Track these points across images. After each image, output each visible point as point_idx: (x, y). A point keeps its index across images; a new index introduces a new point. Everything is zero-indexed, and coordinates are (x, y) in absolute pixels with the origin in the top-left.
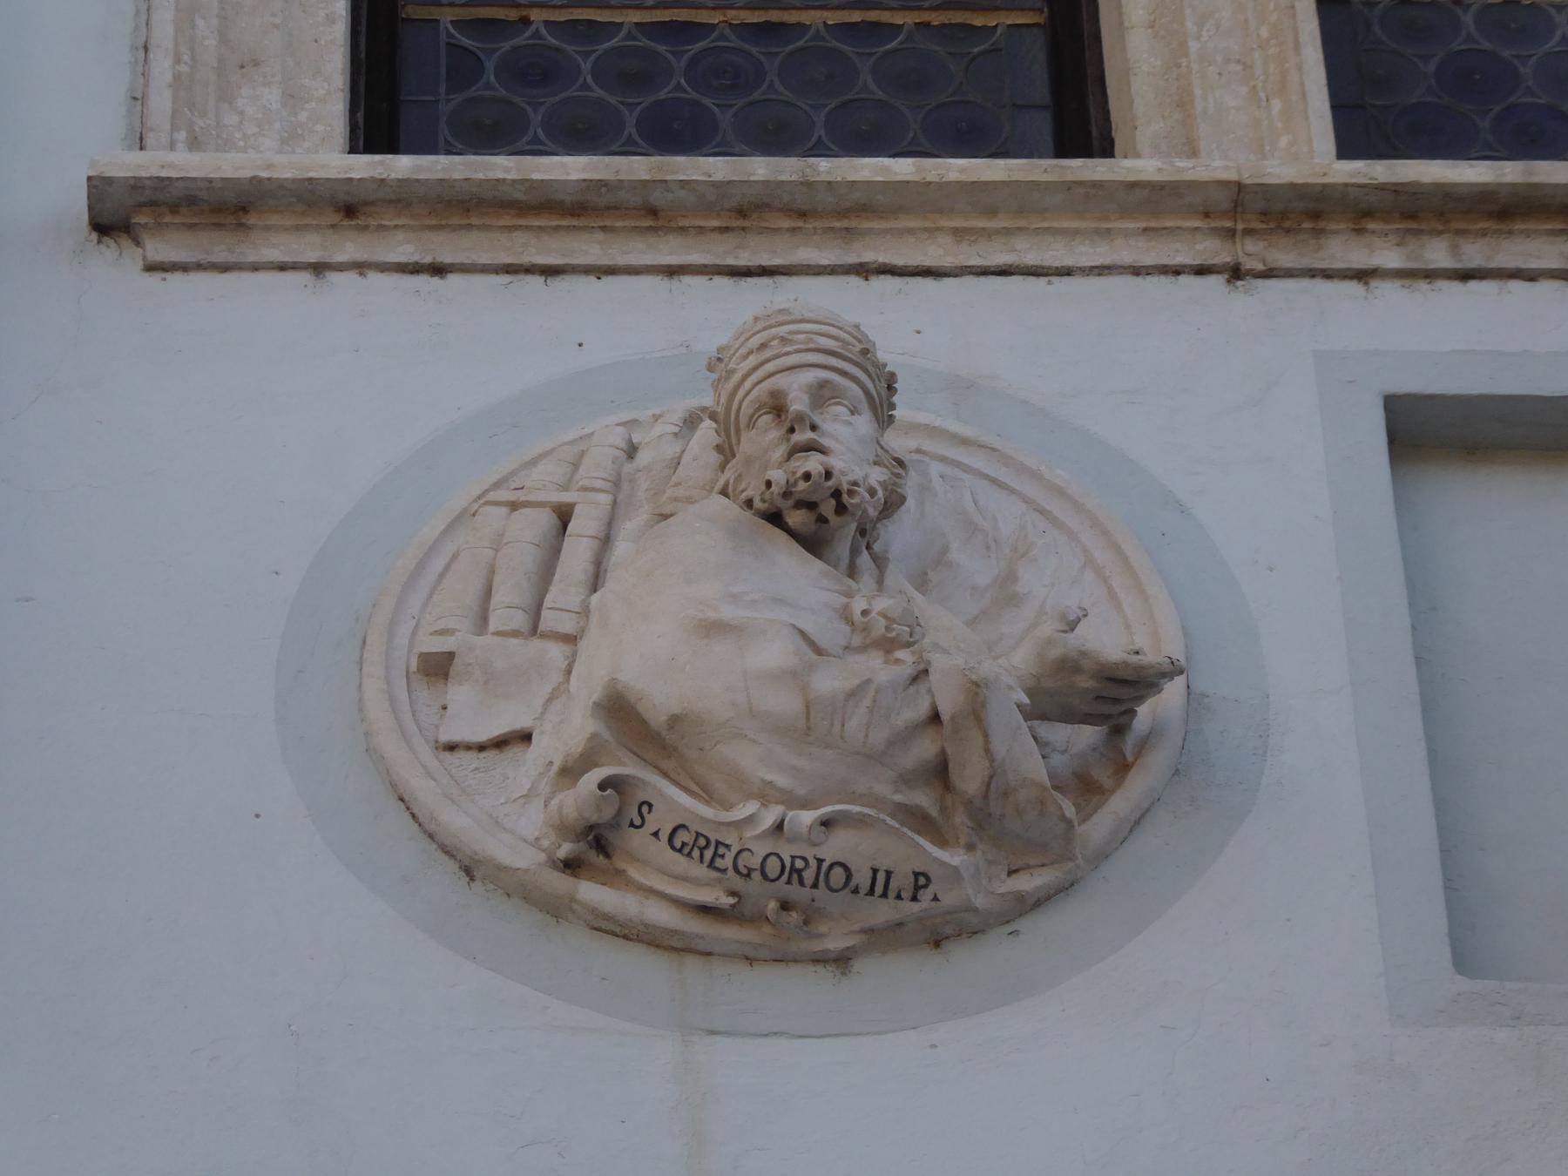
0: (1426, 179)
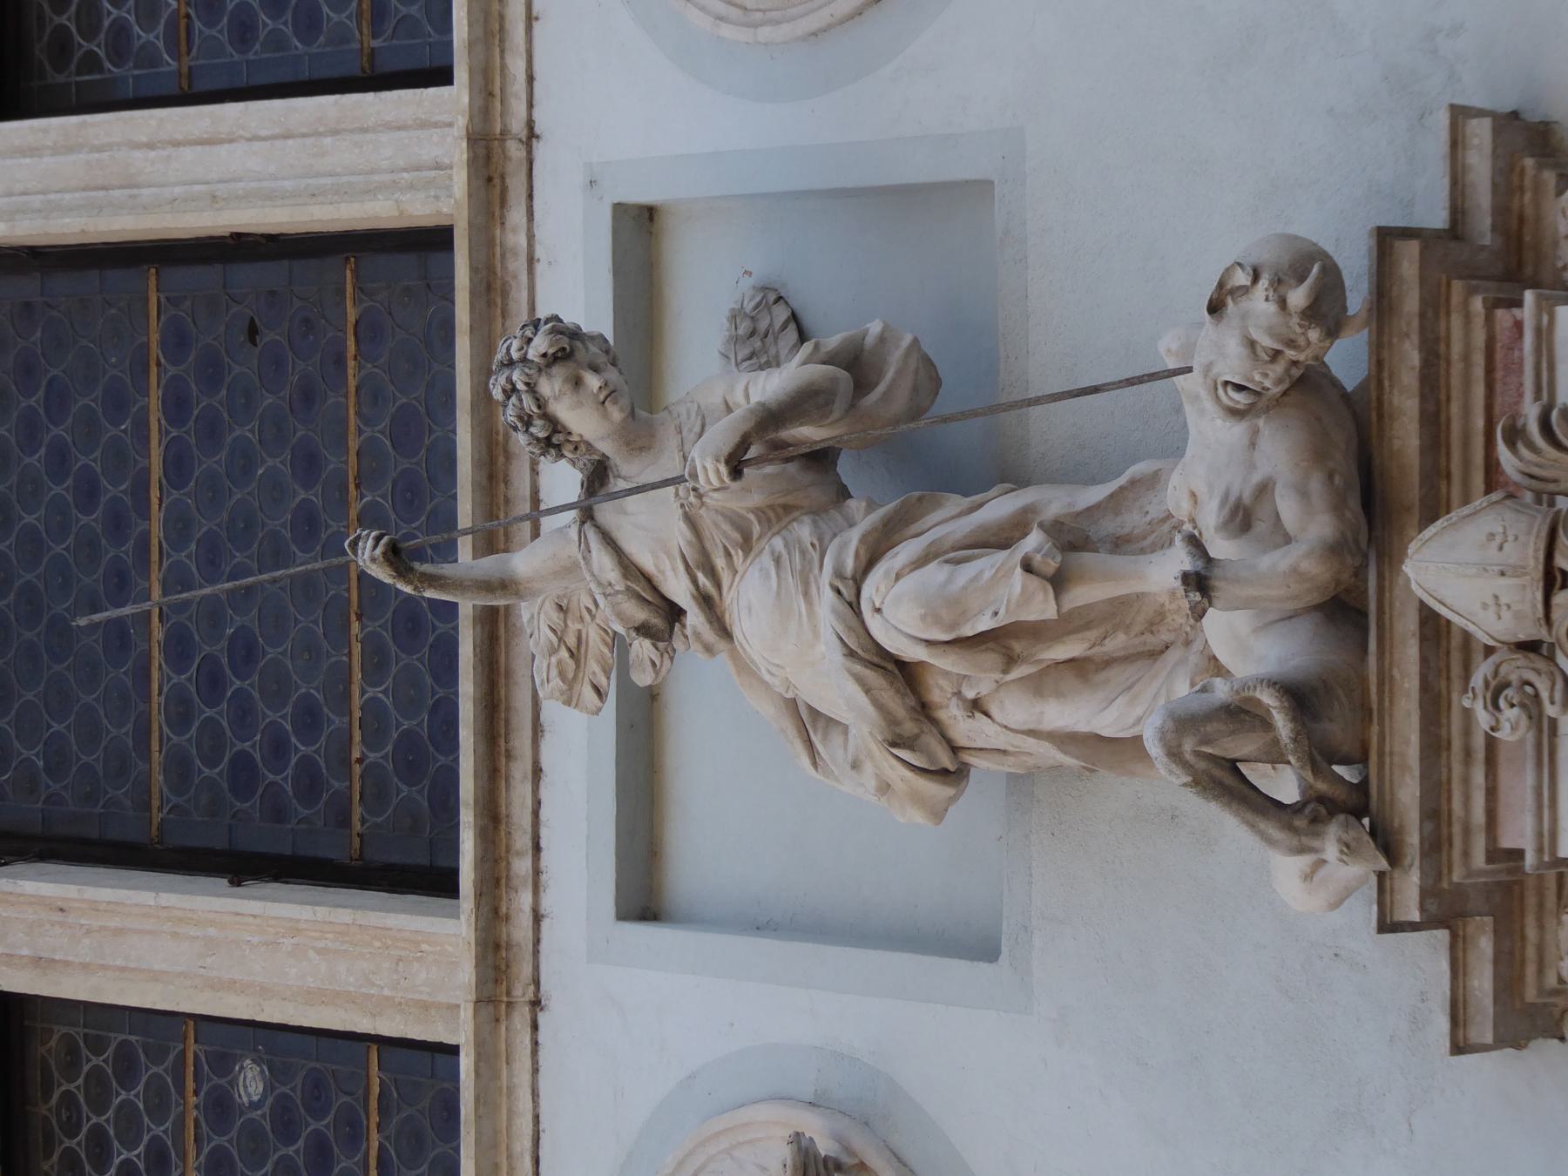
0: (472, 876)
